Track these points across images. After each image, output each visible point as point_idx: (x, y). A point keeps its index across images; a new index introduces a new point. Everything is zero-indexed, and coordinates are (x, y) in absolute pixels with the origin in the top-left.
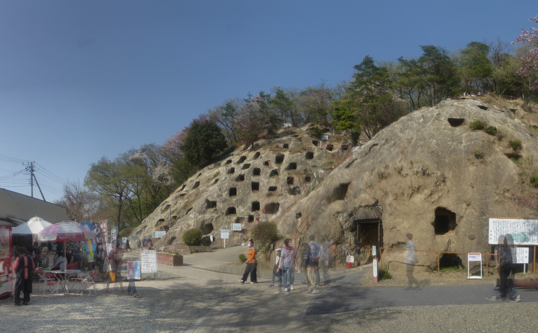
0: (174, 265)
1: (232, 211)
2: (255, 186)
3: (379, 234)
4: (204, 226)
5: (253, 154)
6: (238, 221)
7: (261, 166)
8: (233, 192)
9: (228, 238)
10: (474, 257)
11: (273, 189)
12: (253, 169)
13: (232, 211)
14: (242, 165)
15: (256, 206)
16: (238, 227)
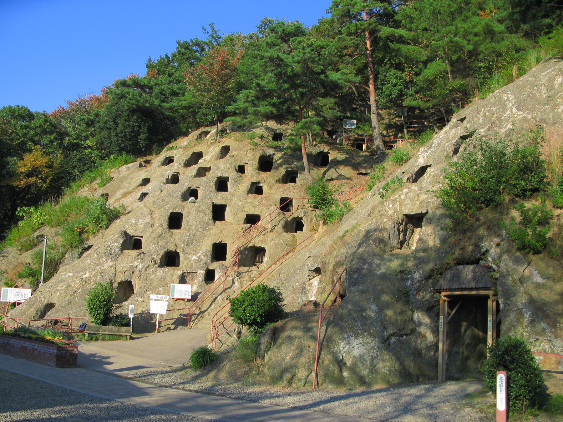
0: (57, 366)
1: (171, 259)
2: (256, 189)
3: (474, 293)
4: (115, 285)
5: (216, 149)
6: (183, 280)
7: (231, 174)
8: (175, 221)
9: (164, 312)
10: (276, 405)
11: (252, 219)
12: (215, 179)
13: (171, 259)
14: (194, 169)
15: (219, 252)
16: (184, 291)
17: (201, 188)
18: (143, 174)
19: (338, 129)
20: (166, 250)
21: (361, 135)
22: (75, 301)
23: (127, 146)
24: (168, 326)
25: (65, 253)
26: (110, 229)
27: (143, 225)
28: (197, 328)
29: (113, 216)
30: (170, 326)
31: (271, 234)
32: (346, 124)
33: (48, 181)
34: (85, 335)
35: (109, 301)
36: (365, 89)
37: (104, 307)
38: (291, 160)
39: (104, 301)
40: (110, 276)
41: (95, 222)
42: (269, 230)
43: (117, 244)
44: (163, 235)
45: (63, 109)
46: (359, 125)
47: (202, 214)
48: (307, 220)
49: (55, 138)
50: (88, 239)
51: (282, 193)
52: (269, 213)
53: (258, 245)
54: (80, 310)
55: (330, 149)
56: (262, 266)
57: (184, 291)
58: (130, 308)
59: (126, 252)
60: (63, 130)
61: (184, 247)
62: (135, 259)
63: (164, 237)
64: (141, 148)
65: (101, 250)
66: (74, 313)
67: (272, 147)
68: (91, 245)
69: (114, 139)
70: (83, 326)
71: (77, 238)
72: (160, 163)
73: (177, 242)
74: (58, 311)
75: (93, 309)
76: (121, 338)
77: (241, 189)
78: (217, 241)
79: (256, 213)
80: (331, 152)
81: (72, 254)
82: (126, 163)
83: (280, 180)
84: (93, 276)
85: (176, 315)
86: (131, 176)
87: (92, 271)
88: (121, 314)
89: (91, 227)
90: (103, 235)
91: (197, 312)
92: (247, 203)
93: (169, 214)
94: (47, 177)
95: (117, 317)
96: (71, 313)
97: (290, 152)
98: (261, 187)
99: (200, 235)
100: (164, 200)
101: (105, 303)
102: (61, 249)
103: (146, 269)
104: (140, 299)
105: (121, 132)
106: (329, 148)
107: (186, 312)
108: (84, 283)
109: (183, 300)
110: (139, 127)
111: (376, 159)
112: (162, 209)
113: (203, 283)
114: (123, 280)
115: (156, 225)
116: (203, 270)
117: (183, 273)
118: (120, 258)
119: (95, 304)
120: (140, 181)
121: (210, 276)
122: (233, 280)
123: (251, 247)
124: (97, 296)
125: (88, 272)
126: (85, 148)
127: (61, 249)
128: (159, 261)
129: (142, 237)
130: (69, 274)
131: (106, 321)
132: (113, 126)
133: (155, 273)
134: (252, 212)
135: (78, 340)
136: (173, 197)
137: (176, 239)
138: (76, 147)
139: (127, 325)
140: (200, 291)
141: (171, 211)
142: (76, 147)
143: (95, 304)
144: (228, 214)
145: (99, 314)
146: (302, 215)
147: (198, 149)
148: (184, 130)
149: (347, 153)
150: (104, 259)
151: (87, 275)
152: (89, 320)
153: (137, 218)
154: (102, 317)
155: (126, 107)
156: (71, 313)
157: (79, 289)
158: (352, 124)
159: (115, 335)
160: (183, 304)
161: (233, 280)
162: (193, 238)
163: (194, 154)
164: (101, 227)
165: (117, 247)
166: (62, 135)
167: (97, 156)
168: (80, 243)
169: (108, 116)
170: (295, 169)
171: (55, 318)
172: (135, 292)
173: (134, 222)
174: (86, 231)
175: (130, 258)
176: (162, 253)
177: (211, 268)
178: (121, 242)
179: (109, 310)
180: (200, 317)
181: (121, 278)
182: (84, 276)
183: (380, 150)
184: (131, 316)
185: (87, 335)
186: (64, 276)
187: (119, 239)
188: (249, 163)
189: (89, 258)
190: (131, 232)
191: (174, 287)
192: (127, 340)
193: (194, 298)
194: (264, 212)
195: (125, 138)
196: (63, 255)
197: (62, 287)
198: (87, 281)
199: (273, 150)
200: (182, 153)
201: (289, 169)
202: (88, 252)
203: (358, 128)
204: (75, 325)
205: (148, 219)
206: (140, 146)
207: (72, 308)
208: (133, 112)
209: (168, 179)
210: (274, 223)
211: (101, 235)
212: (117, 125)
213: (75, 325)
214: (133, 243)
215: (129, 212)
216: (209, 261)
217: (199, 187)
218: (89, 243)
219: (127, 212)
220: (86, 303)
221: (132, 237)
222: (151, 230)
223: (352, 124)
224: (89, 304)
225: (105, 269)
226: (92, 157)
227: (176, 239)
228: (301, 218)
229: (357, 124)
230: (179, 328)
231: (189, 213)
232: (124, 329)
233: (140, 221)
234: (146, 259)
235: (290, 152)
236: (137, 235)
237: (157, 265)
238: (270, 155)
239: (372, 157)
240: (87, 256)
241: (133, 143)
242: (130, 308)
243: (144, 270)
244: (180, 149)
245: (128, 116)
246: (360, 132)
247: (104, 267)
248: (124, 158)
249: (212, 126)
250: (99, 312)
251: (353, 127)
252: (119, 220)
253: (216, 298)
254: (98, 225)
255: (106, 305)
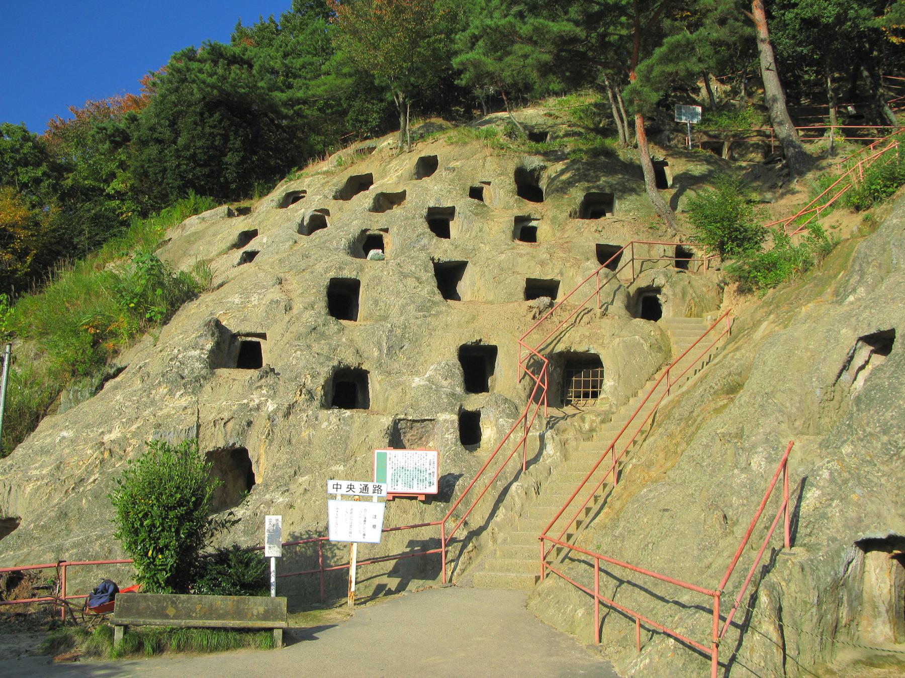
1: (347, 389)
4: (199, 462)
5: (409, 162)
8: (342, 299)
9: (375, 536)
13: (347, 389)
15: (477, 364)
17: (394, 230)
18: (241, 224)
19: (664, 124)
20: (336, 363)
21: (715, 137)
22: (80, 509)
23: (198, 178)
24: (377, 581)
25: (59, 391)
26: (173, 322)
27: (263, 308)
28: (470, 585)
29: (182, 293)
30: (385, 580)
31: (605, 320)
32: (680, 114)
33: (29, 259)
34: (111, 633)
35: (197, 504)
36: (746, 16)
37: (181, 524)
38: (592, 173)
39: (180, 504)
40: (183, 436)
41: (135, 309)
42: (599, 312)
43: (198, 352)
44: (321, 329)
45: (63, 123)
46: (707, 116)
47: (411, 282)
48: (674, 294)
49: (44, 174)
50: (116, 352)
51: (597, 235)
52: (580, 281)
53: (581, 349)
54: (94, 534)
55: (667, 155)
56: (602, 403)
57: (417, 468)
58: (265, 525)
59: (223, 372)
60: (62, 160)
61: (379, 359)
62: (252, 386)
63: (323, 335)
64: (227, 183)
65: (155, 368)
66: (75, 545)
67: (537, 153)
68: (123, 365)
69: (172, 163)
70: (109, 591)
71: (89, 352)
72: (274, 204)
73: (360, 344)
74: (29, 538)
75: (138, 531)
76: (249, 637)
77: (496, 228)
78: (468, 338)
79: (549, 278)
80: (670, 161)
81: (76, 392)
82: (196, 211)
83: (576, 213)
84: (134, 435)
85: (398, 546)
86: (212, 230)
87: (131, 421)
88: (236, 548)
89: (123, 322)
90: (156, 339)
91: (462, 534)
92: (521, 256)
93: (327, 282)
94: (26, 252)
95: (222, 557)
96: (68, 544)
97: (585, 158)
98: (534, 229)
99: (420, 327)
100: (306, 256)
101: (182, 510)
102: (47, 382)
103: (287, 415)
104: (280, 499)
105: (186, 147)
106: (664, 153)
107: (425, 534)
108: (107, 454)
109: (412, 497)
110: (226, 138)
111: (781, 169)
112: (307, 275)
113: (460, 448)
114: (221, 444)
115: (297, 307)
116: (452, 411)
117: (396, 423)
118: (207, 388)
119: (146, 516)
120: (234, 237)
121: (469, 430)
122: (542, 438)
123: (561, 354)
124: (154, 485)
125: (117, 424)
126: (110, 197)
127: (47, 382)
128: (319, 392)
129: (263, 336)
130: (65, 434)
131: (186, 574)
132: (167, 134)
133: (313, 424)
134: (537, 274)
135: (88, 653)
136: (329, 249)
137: (354, 342)
138: (89, 194)
139: (259, 586)
140: (455, 471)
141: (332, 274)
142: (89, 194)
143: (146, 516)
144: (473, 284)
145: (161, 551)
146: (660, 281)
147: (361, 169)
148: (319, 147)
149: (709, 163)
150: (163, 390)
151: (115, 434)
152: (128, 573)
153: (246, 294)
154: (171, 562)
155: (198, 95)
156: (68, 544)
157: (91, 473)
158: (694, 115)
159: (226, 629)
160: (413, 512)
161: (542, 438)
162: (403, 336)
163: (352, 179)
164: (150, 320)
165: (199, 359)
166: (60, 170)
167: (133, 211)
168: (94, 362)
169: (157, 116)
170: (607, 191)
171: (11, 566)
172: (258, 480)
173: (237, 301)
174: (111, 332)
175: (236, 387)
176: (325, 372)
177: (470, 407)
178: (209, 346)
179: (196, 538)
180: (470, 547)
181: (214, 440)
182: (107, 438)
183: (794, 147)
184: (272, 552)
185: (119, 634)
186: (49, 440)
187: (202, 341)
188: (495, 181)
189: (116, 395)
190: (232, 325)
191: (383, 459)
192: (272, 646)
193: (446, 489)
194: (570, 273)
195: (195, 162)
196: (53, 397)
197: (41, 469)
198: (117, 449)
199: (541, 158)
200: (323, 181)
201: (593, 191)
202: (118, 379)
203: (704, 121)
204: (75, 589)
205: (275, 294)
206: (226, 178)
207: (69, 531)
208: (211, 106)
209: (301, 225)
210: (604, 297)
211: (152, 339)
212: (177, 133)
213: (75, 589)
214: (244, 353)
215: (221, 285)
216: (459, 390)
217: (386, 230)
218: (118, 362)
219: (216, 282)
220: (114, 513)
221: (235, 336)
222: (287, 318)
223: (694, 115)
224: (126, 515)
225: (168, 416)
226: (122, 214)
227: (354, 342)
228: (658, 290)
229: (703, 114)
230: (414, 585)
231: (377, 280)
232: (256, 604)
233: (255, 299)
234: (281, 389)
235: (585, 158)
236: (248, 330)
237: (317, 403)
238: (534, 170)
239: (770, 166)
240: (116, 388)
241: (212, 171)
242: (265, 525)
243: (280, 414)
244: (317, 181)
245: (202, 114)
246: (713, 130)
247: (165, 411)
248: (192, 201)
249: (378, 137)
250: (161, 543)
251: (695, 121)
252: (196, 303)
253: (506, 490)
254: (142, 316)
255: (187, 517)
